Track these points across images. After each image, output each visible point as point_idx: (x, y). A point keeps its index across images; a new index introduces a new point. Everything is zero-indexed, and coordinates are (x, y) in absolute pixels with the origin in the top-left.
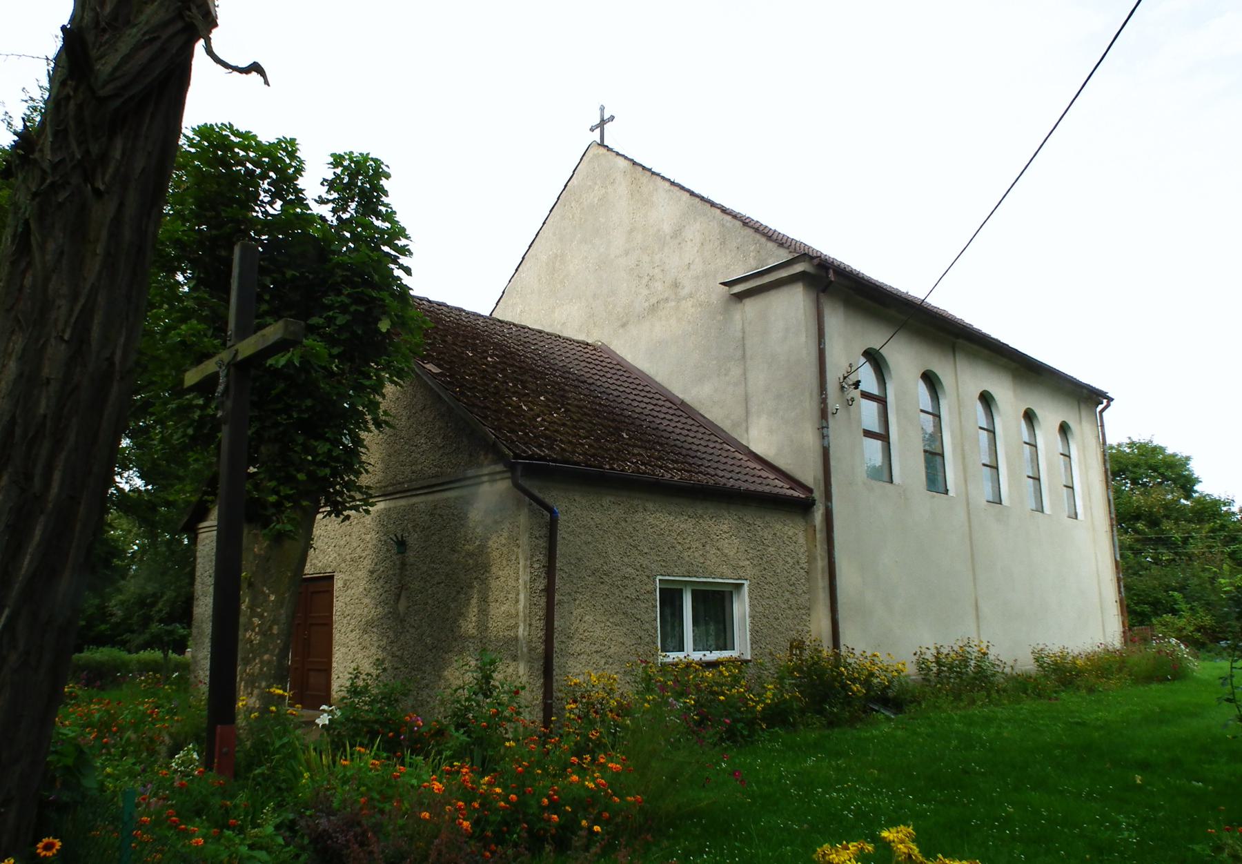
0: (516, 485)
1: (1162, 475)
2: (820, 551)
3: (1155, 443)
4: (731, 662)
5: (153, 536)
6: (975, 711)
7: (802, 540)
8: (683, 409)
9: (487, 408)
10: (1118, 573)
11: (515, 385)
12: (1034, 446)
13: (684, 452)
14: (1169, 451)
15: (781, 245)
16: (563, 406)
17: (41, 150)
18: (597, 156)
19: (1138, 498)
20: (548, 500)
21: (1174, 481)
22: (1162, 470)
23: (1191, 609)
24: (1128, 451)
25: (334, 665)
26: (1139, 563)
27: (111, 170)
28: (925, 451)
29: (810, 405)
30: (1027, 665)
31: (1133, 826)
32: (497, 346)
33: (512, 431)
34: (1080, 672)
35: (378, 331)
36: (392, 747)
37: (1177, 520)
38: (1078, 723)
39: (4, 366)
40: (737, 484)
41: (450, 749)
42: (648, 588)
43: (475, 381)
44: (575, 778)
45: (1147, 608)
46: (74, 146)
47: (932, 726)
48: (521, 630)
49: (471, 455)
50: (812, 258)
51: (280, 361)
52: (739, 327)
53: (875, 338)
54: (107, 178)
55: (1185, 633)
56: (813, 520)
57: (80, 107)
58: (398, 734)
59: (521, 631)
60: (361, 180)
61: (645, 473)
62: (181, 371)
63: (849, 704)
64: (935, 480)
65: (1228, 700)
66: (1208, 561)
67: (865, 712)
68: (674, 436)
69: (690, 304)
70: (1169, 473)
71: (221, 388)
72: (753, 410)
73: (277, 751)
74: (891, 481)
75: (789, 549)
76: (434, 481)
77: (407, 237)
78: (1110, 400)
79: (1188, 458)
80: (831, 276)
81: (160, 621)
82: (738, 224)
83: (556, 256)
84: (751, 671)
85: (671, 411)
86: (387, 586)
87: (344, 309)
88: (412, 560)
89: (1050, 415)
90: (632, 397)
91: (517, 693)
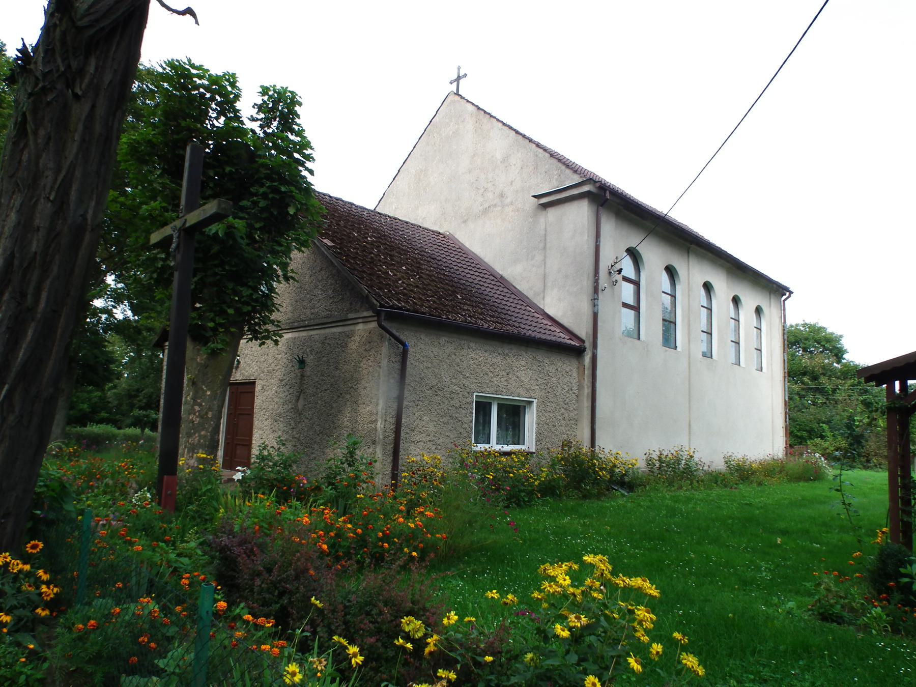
0: (380, 326)
1: (823, 346)
2: (587, 382)
3: (820, 325)
4: (520, 452)
5: (138, 352)
6: (681, 493)
7: (575, 375)
8: (501, 281)
9: (364, 272)
11: (385, 258)
12: (737, 320)
13: (499, 310)
14: (829, 331)
15: (575, 172)
16: (418, 274)
17: (36, 63)
18: (453, 102)
19: (806, 361)
20: (402, 337)
21: (831, 351)
22: (823, 343)
23: (833, 436)
24: (802, 329)
25: (254, 442)
26: (803, 404)
27: (86, 81)
28: (664, 320)
29: (587, 283)
30: (719, 465)
31: (770, 570)
32: (375, 230)
33: (380, 289)
34: (754, 473)
35: (288, 213)
36: (283, 498)
37: (830, 377)
38: (747, 504)
39: (7, 216)
40: (533, 334)
41: (323, 498)
42: (469, 400)
43: (357, 253)
44: (401, 520)
45: (805, 434)
46: (59, 60)
47: (651, 501)
48: (379, 423)
49: (351, 304)
50: (595, 182)
51: (214, 228)
52: (543, 227)
53: (633, 239)
54: (84, 86)
56: (584, 361)
57: (64, 34)
58: (290, 488)
59: (380, 425)
60: (281, 107)
61: (470, 322)
62: (148, 233)
63: (598, 484)
64: (669, 339)
65: (837, 490)
66: (847, 405)
67: (608, 490)
68: (493, 299)
69: (511, 209)
70: (827, 345)
71: (174, 246)
72: (549, 284)
73: (204, 494)
74: (639, 339)
75: (566, 380)
76: (325, 320)
77: (312, 149)
78: (791, 293)
79: (841, 336)
80: (608, 195)
81: (140, 408)
82: (547, 155)
83: (421, 171)
84: (533, 460)
85: (493, 283)
86: (291, 390)
87: (264, 196)
88: (308, 374)
89: (751, 299)
90: (467, 271)
91: (370, 464)
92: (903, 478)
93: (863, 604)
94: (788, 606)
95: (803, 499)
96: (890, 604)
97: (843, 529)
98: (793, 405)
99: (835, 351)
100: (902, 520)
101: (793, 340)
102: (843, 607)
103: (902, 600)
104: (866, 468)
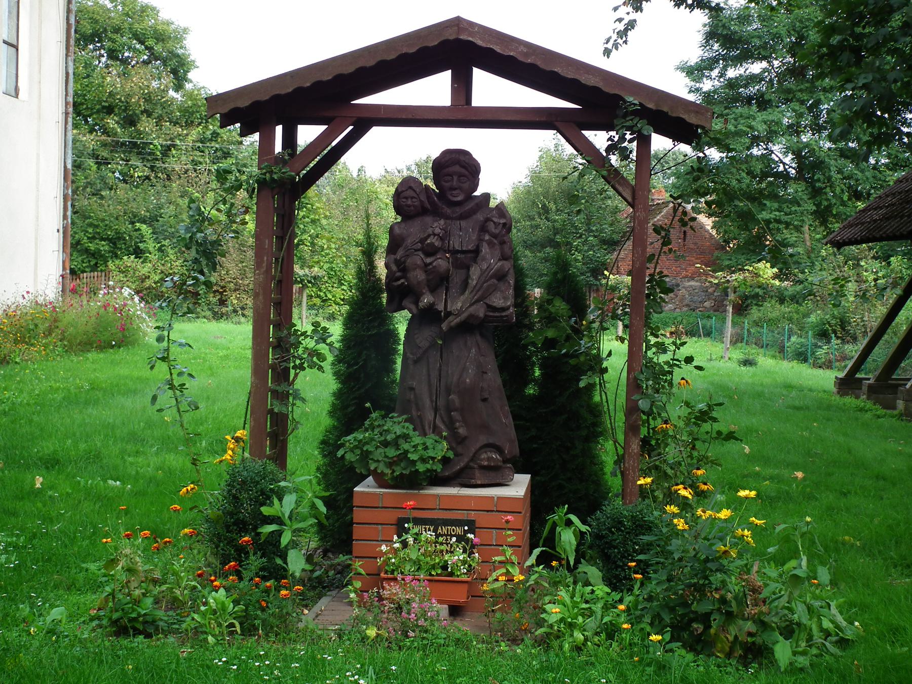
10: (66, 187)
19: (112, 80)
22: (150, 43)
23: (160, 250)
26: (103, 179)
37: (160, 119)
45: (104, 247)
55: (148, 283)
70: (158, 48)
79: (185, 30)
92: (278, 326)
93: (195, 588)
94: (49, 619)
95: (94, 387)
96: (241, 579)
97: (167, 444)
98: (82, 180)
99: (173, 63)
100: (271, 412)
101: (88, 29)
102: (157, 602)
103: (262, 569)
104: (218, 316)
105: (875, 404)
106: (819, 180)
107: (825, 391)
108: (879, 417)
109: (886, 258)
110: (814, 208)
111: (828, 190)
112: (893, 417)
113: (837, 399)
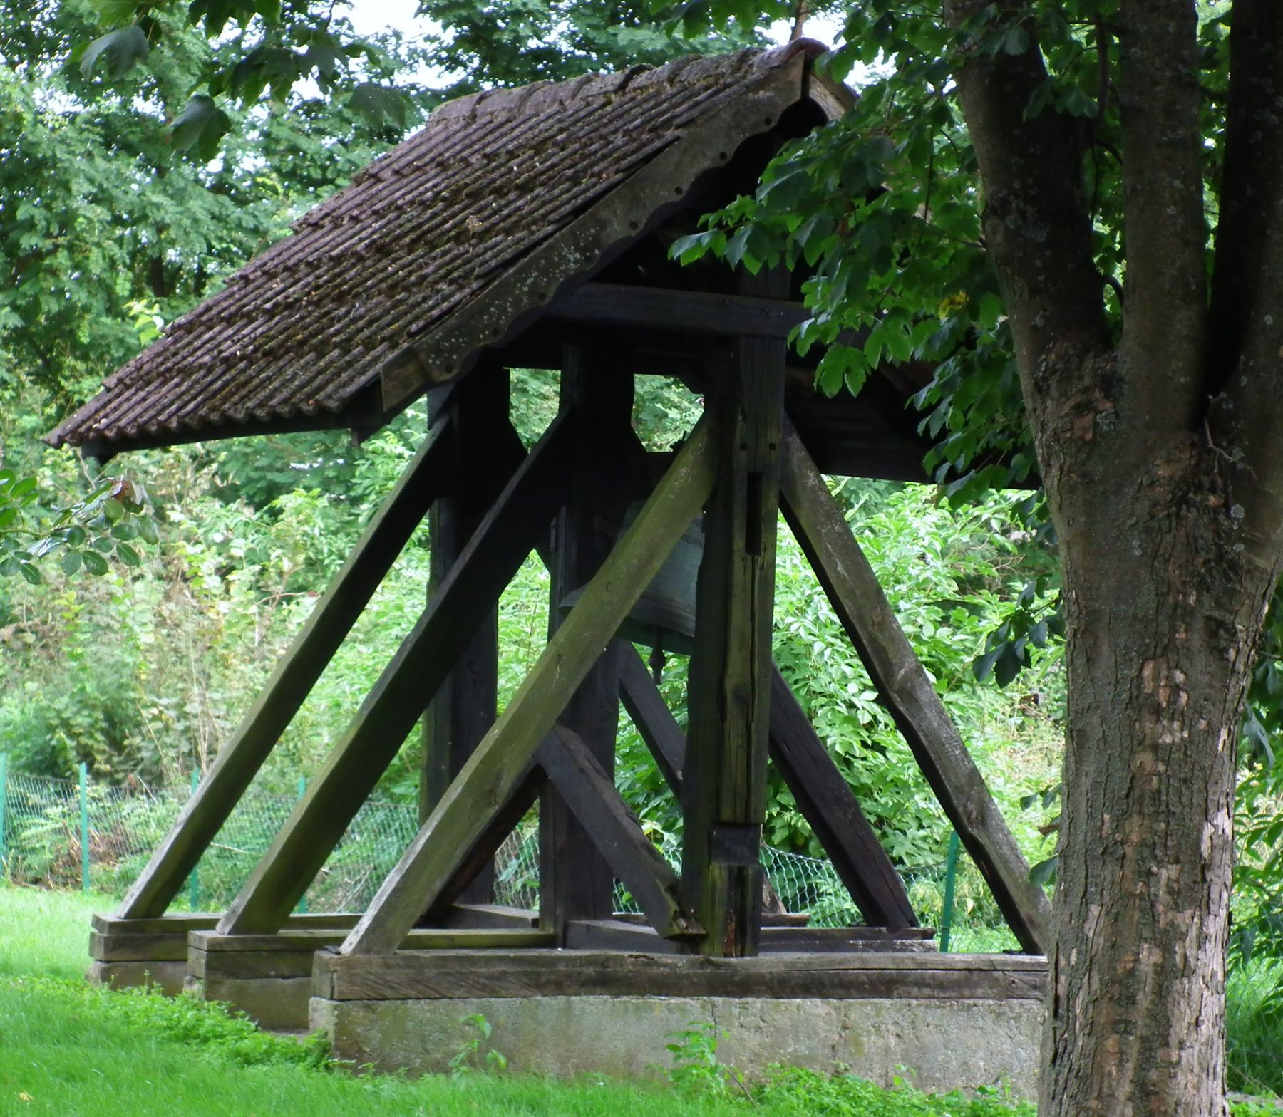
105: (232, 1014)
106: (30, 225)
107: (56, 972)
108: (247, 1060)
109: (264, 497)
110: (15, 321)
111: (62, 258)
112: (296, 1058)
113: (101, 1002)
